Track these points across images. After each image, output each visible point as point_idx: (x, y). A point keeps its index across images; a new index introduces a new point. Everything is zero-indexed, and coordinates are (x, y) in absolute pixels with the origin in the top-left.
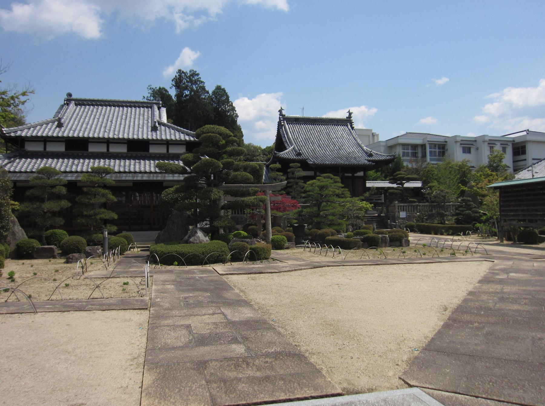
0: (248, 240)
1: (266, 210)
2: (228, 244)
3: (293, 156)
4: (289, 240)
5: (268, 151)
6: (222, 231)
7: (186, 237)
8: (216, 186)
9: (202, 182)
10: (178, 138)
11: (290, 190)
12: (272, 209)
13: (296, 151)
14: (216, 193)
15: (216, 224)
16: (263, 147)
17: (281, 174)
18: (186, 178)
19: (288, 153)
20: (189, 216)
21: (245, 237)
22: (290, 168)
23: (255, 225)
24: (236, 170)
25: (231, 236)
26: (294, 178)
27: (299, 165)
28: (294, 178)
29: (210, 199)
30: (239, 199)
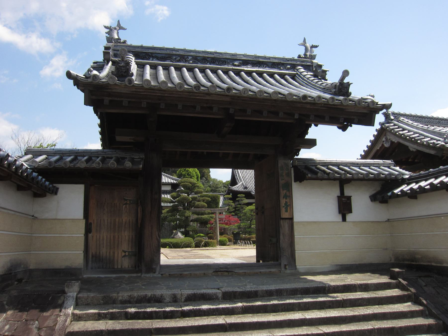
0: (204, 238)
1: (216, 223)
2: (194, 239)
3: (241, 189)
4: (230, 240)
5: (225, 185)
6: (191, 233)
7: (172, 236)
8: (188, 209)
9: (181, 208)
10: (167, 181)
11: (238, 212)
12: (219, 224)
13: (244, 186)
14: (188, 213)
15: (187, 229)
16: (224, 181)
17: (232, 201)
18: (408, 294)
19: (238, 187)
20: (174, 226)
21: (203, 236)
22: (238, 197)
23: (213, 234)
24: (199, 201)
25: (195, 236)
26: (240, 204)
27: (244, 195)
28: (240, 204)
29: (185, 216)
30: (200, 216)
